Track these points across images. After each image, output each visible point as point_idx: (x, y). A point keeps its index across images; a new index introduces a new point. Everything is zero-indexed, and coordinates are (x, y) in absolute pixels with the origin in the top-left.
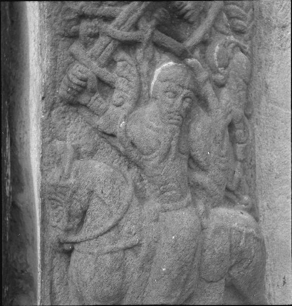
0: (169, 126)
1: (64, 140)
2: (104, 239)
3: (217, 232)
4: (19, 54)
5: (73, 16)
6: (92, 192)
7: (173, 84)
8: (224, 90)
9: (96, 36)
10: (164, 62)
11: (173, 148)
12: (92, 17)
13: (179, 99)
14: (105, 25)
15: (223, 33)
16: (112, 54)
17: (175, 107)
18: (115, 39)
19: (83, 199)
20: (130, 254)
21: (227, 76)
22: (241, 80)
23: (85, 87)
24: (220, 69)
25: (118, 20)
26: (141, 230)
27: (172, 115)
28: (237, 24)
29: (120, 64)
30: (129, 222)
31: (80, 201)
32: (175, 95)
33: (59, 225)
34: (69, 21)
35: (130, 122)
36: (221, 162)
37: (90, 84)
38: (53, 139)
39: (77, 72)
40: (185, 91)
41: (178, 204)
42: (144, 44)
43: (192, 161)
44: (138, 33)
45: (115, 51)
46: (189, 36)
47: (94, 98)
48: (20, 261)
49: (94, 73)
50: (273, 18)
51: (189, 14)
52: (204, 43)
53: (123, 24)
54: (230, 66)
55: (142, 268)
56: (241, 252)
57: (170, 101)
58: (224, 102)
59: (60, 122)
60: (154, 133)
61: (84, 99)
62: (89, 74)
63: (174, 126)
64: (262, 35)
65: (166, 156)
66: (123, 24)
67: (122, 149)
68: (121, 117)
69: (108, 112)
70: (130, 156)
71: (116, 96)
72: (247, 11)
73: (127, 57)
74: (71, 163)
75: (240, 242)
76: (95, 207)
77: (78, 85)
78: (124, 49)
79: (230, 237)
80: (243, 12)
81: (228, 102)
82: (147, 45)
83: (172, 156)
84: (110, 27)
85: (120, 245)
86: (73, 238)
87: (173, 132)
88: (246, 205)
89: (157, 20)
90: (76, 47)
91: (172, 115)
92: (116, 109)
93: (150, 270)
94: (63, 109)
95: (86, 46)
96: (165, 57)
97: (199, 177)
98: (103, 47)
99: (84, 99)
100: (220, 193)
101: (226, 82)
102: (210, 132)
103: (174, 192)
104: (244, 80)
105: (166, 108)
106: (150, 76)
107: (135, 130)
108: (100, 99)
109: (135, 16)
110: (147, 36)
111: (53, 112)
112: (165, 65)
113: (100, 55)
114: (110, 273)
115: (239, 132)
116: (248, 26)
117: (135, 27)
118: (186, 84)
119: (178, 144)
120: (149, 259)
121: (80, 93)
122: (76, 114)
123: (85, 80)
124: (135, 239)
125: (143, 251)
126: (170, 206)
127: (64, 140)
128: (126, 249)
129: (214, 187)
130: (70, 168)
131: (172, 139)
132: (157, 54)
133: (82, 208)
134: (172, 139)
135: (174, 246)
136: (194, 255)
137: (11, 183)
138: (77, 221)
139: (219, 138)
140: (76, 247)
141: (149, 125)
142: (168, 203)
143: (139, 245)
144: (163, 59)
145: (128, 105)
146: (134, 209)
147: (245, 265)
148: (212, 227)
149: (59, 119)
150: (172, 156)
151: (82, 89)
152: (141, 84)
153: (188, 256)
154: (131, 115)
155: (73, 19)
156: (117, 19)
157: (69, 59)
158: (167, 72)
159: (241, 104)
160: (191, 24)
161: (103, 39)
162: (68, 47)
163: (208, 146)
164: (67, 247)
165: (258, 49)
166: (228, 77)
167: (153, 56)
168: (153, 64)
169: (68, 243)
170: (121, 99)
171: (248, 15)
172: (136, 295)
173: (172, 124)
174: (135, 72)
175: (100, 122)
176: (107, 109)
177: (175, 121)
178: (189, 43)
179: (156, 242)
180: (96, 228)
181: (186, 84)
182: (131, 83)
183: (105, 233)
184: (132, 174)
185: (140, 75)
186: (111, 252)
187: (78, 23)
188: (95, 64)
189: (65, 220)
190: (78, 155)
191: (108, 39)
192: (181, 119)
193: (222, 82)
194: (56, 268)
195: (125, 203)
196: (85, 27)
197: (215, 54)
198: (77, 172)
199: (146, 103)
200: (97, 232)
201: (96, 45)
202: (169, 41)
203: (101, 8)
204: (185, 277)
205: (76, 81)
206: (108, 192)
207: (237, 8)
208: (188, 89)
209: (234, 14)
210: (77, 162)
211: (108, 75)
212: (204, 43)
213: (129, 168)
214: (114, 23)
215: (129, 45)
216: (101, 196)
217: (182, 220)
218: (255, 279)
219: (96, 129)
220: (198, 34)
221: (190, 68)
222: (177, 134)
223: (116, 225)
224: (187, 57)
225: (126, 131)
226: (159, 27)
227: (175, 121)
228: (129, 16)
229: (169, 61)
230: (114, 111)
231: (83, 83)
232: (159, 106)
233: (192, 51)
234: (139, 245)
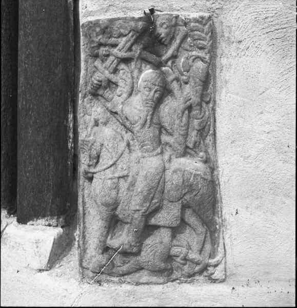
0: (146, 108)
1: (91, 115)
2: (108, 171)
3: (175, 172)
5: (95, 45)
6: (103, 144)
7: (149, 83)
8: (188, 86)
9: (108, 56)
10: (147, 70)
11: (149, 121)
12: (105, 45)
13: (153, 92)
14: (112, 49)
15: (187, 50)
16: (117, 66)
17: (149, 97)
18: (118, 58)
19: (97, 148)
20: (122, 180)
21: (189, 77)
22: (198, 80)
23: (101, 85)
24: (184, 73)
25: (120, 46)
26: (129, 168)
27: (148, 101)
28: (199, 43)
29: (121, 71)
30: (122, 163)
31: (95, 149)
32: (150, 89)
33: (85, 163)
34: (93, 47)
35: (125, 105)
36: (180, 130)
37: (103, 84)
38: (85, 115)
39: (98, 76)
40: (156, 87)
41: (151, 154)
42: (135, 59)
43: (161, 128)
44: (133, 53)
46: (165, 53)
49: (106, 77)
50: (232, 36)
51: (164, 40)
52: (174, 57)
53: (122, 49)
54: (191, 71)
55: (128, 189)
56: (191, 186)
57: (147, 93)
58: (185, 93)
59: (88, 105)
60: (138, 112)
61: (101, 92)
62: (102, 77)
63: (149, 108)
64: (224, 48)
65: (144, 125)
66: (122, 49)
67: (121, 121)
68: (120, 102)
69: (114, 100)
71: (118, 91)
72: (207, 34)
74: (92, 128)
75: (190, 179)
76: (104, 154)
77: (96, 84)
79: (183, 175)
80: (204, 35)
81: (188, 93)
82: (137, 60)
83: (147, 125)
84: (115, 51)
85: (116, 175)
86: (92, 170)
87: (148, 111)
88: (201, 158)
89: (143, 45)
90: (98, 63)
91: (148, 101)
92: (118, 98)
93: (133, 190)
94: (90, 97)
95: (103, 61)
96: (148, 66)
97: (165, 138)
98: (111, 62)
99: (101, 92)
100: (181, 149)
101: (189, 81)
102: (175, 111)
103: (149, 147)
104: (200, 80)
105: (145, 97)
106: (138, 78)
107: (127, 110)
108: (109, 92)
109: (129, 43)
110: (137, 55)
111: (85, 100)
112: (147, 72)
113: (109, 67)
114: (110, 190)
116: (208, 44)
117: (130, 49)
118: (157, 83)
119: (152, 119)
120: (133, 184)
121: (98, 88)
122: (97, 101)
123: (101, 81)
124: (125, 173)
125: (130, 179)
126: (146, 155)
127: (91, 115)
128: (119, 178)
129: (176, 145)
130: (91, 131)
131: (147, 116)
132: (143, 65)
133: (97, 154)
134: (147, 116)
135: (146, 177)
136: (159, 183)
137: (72, 142)
138: (95, 161)
139: (180, 115)
140: (95, 175)
141: (136, 108)
142: (145, 153)
143: (127, 176)
144: (147, 68)
145: (125, 95)
146: (126, 155)
147: (194, 193)
148: (173, 168)
149: (88, 104)
150: (147, 125)
151: (99, 86)
152: (133, 83)
153: (154, 183)
154: (125, 102)
156: (119, 46)
157: (94, 69)
158: (147, 76)
159: (198, 94)
160: (166, 46)
161: (112, 58)
162: (94, 62)
163: (173, 121)
164: (90, 175)
165: (221, 57)
166: (190, 78)
167: (141, 66)
168: (140, 71)
169: (90, 173)
170: (121, 92)
171: (208, 37)
172: (125, 204)
173: (147, 106)
174: (130, 76)
175: (109, 105)
176: (113, 98)
178: (164, 58)
179: (137, 175)
180: (104, 165)
181: (157, 83)
182: (127, 83)
183: (108, 168)
184: (128, 136)
185: (133, 78)
186: (111, 179)
187: (99, 48)
188: (107, 72)
189: (88, 159)
190: (96, 124)
191: (114, 57)
192: (154, 104)
193: (187, 81)
194: (86, 188)
195: (120, 152)
196: (102, 51)
197: (181, 64)
198: (95, 133)
199: (137, 94)
200: (105, 167)
201: (108, 61)
202: (152, 58)
203: (111, 39)
204: (152, 195)
205: (96, 82)
206: (110, 145)
207: (199, 33)
208: (158, 86)
210: (96, 128)
211: (114, 78)
212: (174, 57)
213: (126, 132)
214: (118, 48)
215: (126, 61)
216: (107, 147)
217: (152, 163)
218: (203, 203)
220: (170, 52)
221: (163, 73)
222: (151, 113)
223: (114, 164)
224: (162, 66)
225: (122, 111)
226: (144, 48)
228: (126, 43)
229: (149, 69)
230: (117, 98)
231: (99, 83)
232: (142, 96)
233: (167, 62)
234: (127, 176)
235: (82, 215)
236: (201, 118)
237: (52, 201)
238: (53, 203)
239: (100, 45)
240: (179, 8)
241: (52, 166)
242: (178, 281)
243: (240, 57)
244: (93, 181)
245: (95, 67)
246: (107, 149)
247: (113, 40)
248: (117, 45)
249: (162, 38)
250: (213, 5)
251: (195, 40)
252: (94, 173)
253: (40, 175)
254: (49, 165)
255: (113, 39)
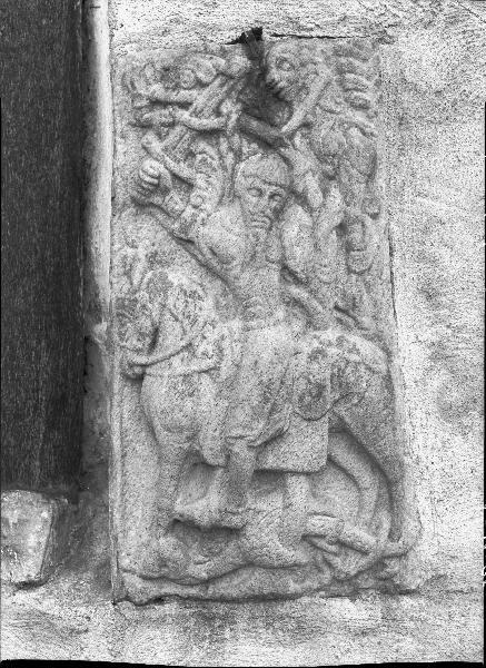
4: (95, 135)
9: (172, 125)
12: (164, 104)
15: (332, 112)
45: (193, 139)
47: (168, 198)
48: (99, 421)
57: (254, 200)
70: (214, 267)
73: (208, 149)
78: (204, 138)
110: (231, 124)
115: (356, 236)
140: (148, 370)
155: (146, 106)
161: (178, 129)
164: (137, 370)
177: (261, 224)
209: (350, 86)
219: (171, 233)
227: (261, 224)
231: (156, 181)
235: (118, 457)
236: (206, 583)
237: (44, 436)
238: (46, 440)
239: (155, 103)
240: (313, 26)
241: (45, 359)
242: (322, 593)
243: (247, 236)
244: (144, 383)
245: (144, 148)
246: (172, 314)
247: (183, 95)
248: (191, 104)
249: (282, 89)
250: (382, 19)
251: (348, 90)
252: (144, 366)
253: (18, 380)
254: (38, 357)
255: (182, 92)
